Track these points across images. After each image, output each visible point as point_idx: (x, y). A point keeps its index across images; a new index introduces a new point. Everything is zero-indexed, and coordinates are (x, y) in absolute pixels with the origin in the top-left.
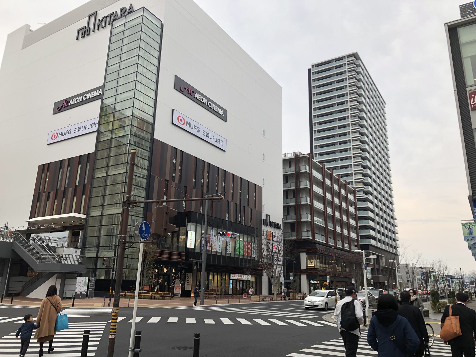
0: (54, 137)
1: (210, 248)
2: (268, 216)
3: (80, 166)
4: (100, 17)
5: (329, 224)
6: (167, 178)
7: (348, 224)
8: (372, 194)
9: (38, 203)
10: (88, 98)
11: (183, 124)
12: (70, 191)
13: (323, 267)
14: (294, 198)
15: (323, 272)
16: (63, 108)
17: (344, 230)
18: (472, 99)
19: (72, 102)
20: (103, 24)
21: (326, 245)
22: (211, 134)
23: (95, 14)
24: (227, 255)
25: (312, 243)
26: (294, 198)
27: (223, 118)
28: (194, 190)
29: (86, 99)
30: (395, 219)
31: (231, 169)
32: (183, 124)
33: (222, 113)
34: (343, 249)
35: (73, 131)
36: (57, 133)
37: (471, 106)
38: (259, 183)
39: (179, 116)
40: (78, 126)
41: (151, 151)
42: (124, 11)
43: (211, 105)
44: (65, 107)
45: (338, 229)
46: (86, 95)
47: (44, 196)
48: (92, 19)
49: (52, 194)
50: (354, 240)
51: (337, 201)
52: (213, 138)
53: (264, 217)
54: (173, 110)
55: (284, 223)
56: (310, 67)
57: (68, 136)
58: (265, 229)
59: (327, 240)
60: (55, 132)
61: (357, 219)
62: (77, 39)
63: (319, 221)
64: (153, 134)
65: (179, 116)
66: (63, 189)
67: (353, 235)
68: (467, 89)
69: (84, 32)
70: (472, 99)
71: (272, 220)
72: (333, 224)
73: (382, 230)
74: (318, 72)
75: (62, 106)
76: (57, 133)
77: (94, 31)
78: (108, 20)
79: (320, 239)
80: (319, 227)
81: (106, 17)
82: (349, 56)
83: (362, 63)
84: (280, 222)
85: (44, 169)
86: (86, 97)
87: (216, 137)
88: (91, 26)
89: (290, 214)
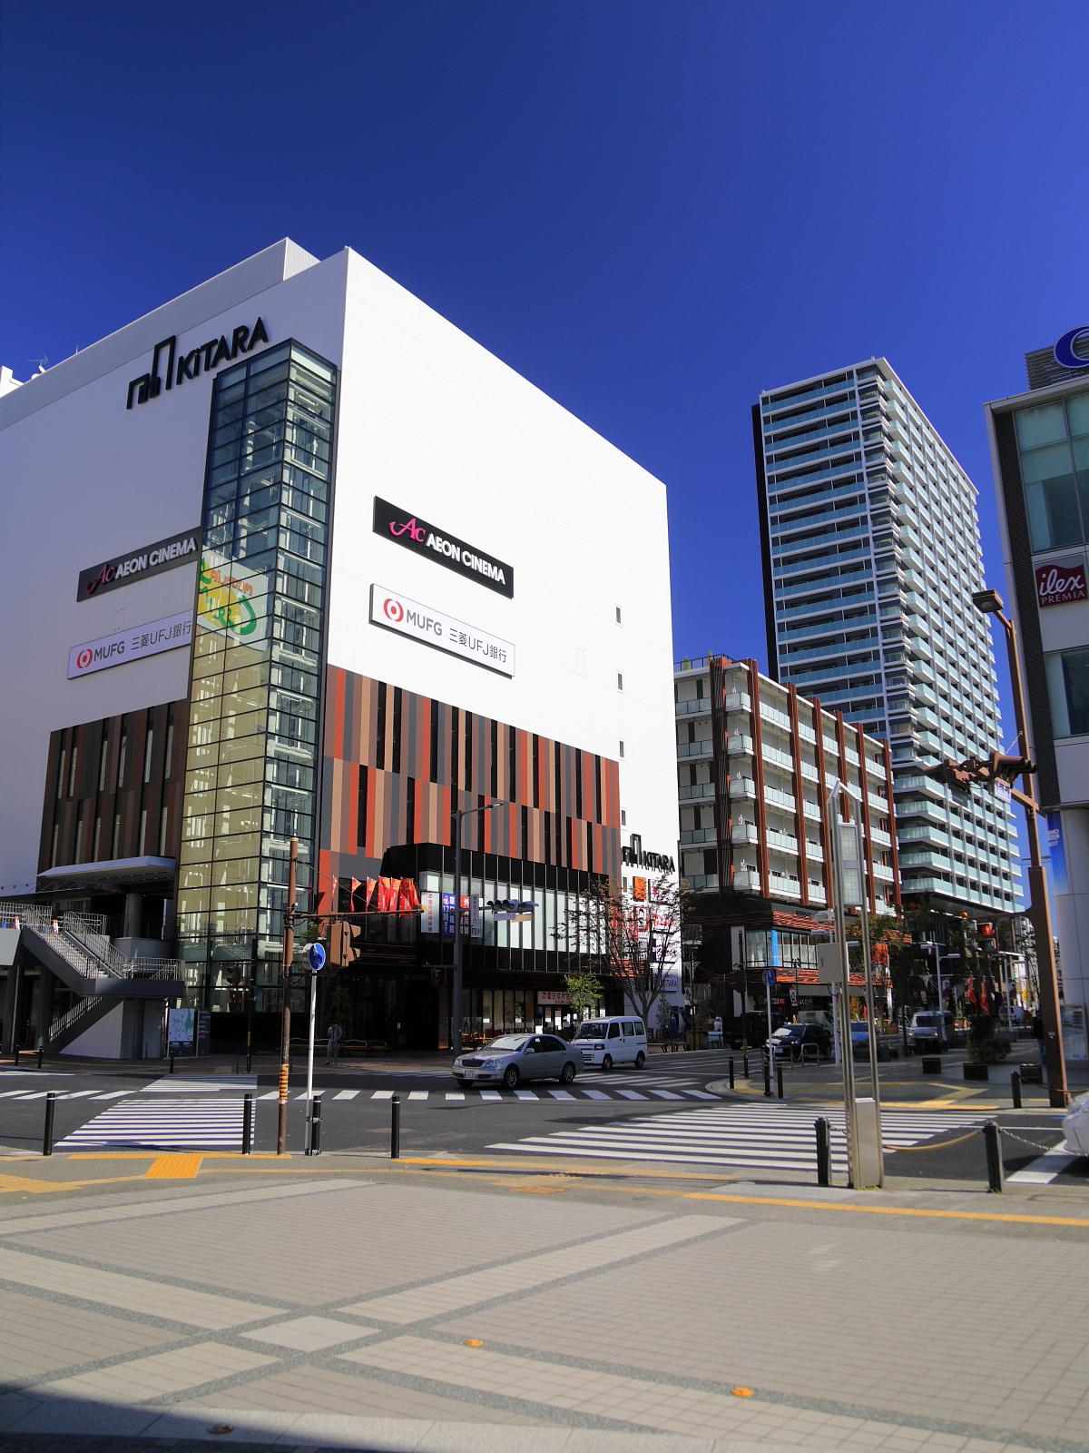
0: (85, 659)
1: (467, 929)
2: (636, 838)
3: (151, 733)
10: (160, 560)
12: (131, 798)
16: (100, 587)
18: (1043, 584)
19: (122, 571)
20: (192, 365)
22: (473, 635)
23: (172, 341)
27: (506, 589)
28: (433, 786)
29: (158, 564)
31: (528, 723)
33: (499, 576)
35: (128, 645)
36: (90, 651)
37: (1041, 601)
38: (608, 752)
39: (387, 602)
40: (140, 633)
41: (320, 699)
42: (241, 335)
43: (468, 560)
44: (106, 582)
46: (155, 553)
47: (69, 809)
48: (166, 352)
49: (88, 806)
52: (478, 644)
53: (625, 841)
55: (682, 854)
57: (116, 658)
58: (629, 871)
59: (804, 891)
60: (85, 648)
62: (130, 406)
64: (322, 653)
65: (387, 602)
66: (113, 791)
68: (1034, 559)
69: (148, 388)
70: (1043, 584)
71: (647, 847)
75: (95, 582)
76: (90, 651)
77: (169, 387)
78: (203, 355)
80: (781, 858)
81: (198, 351)
84: (672, 852)
85: (63, 740)
86: (156, 557)
87: (487, 641)
88: (163, 373)
89: (704, 825)
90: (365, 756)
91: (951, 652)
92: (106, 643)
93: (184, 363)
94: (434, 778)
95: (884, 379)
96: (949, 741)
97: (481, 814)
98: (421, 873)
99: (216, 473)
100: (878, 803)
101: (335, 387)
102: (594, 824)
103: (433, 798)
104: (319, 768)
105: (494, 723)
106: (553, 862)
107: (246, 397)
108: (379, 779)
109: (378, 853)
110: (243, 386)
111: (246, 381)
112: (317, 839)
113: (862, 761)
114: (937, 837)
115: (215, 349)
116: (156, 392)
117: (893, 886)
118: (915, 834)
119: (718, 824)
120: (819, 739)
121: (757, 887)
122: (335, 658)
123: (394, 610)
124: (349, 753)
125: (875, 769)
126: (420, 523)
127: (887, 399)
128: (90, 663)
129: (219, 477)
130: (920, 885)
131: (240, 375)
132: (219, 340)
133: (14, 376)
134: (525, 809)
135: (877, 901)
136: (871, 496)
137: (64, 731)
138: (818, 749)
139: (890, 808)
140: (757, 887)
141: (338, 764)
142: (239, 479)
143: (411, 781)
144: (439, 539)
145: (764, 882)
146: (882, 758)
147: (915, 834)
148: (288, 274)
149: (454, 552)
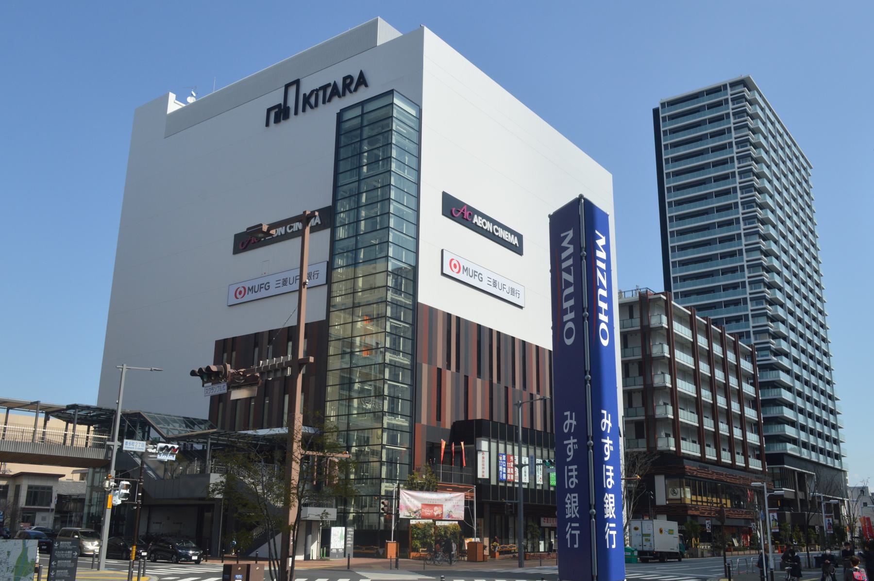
4: (305, 89)
5: (705, 420)
6: (440, 365)
7: (742, 417)
8: (787, 355)
9: (221, 404)
11: (459, 272)
13: (697, 501)
14: (640, 375)
15: (697, 510)
17: (735, 429)
21: (702, 459)
22: (500, 281)
23: (297, 83)
24: (538, 488)
25: (678, 457)
26: (640, 375)
28: (479, 381)
30: (837, 399)
32: (459, 272)
33: (515, 241)
34: (733, 466)
35: (273, 285)
36: (244, 288)
39: (452, 260)
41: (414, 325)
42: (348, 81)
43: (497, 231)
45: (723, 429)
48: (292, 90)
50: (754, 448)
51: (719, 375)
54: (442, 251)
56: (658, 105)
57: (263, 293)
59: (703, 451)
60: (240, 285)
61: (759, 404)
62: (267, 124)
63: (688, 417)
65: (452, 260)
67: (753, 438)
69: (280, 113)
72: (714, 419)
73: (810, 423)
74: (673, 117)
75: (249, 240)
76: (244, 288)
77: (296, 113)
78: (321, 93)
79: (690, 448)
80: (688, 428)
81: (317, 90)
82: (733, 85)
83: (761, 95)
86: (291, 227)
87: (509, 285)
88: (291, 103)
89: (634, 405)
90: (440, 363)
91: (795, 282)
92: (256, 283)
93: (306, 99)
94: (479, 374)
95: (749, 90)
96: (795, 345)
97: (532, 404)
98: (478, 439)
99: (341, 176)
100: (748, 389)
101: (419, 118)
102: (510, 388)
103: (479, 387)
104: (414, 370)
105: (513, 338)
106: (549, 430)
107: (361, 127)
108: (448, 376)
109: (448, 426)
110: (360, 119)
111: (362, 115)
112: (414, 417)
113: (738, 360)
114: (788, 413)
115: (329, 91)
116: (286, 116)
117: (760, 448)
118: (774, 412)
119: (644, 404)
120: (724, 353)
121: (673, 448)
122: (421, 299)
123: (455, 266)
124: (431, 361)
125: (746, 366)
126: (469, 208)
127: (751, 105)
128: (244, 295)
129: (343, 179)
130: (777, 448)
131: (358, 111)
132: (332, 83)
133: (177, 99)
134: (532, 395)
135: (707, 449)
136: (740, 173)
137: (225, 340)
138: (710, 352)
139: (757, 393)
140: (673, 448)
141: (425, 367)
142: (359, 181)
143: (466, 377)
144: (480, 218)
145: (678, 445)
146: (751, 357)
147: (774, 412)
148: (380, 42)
149: (489, 226)
